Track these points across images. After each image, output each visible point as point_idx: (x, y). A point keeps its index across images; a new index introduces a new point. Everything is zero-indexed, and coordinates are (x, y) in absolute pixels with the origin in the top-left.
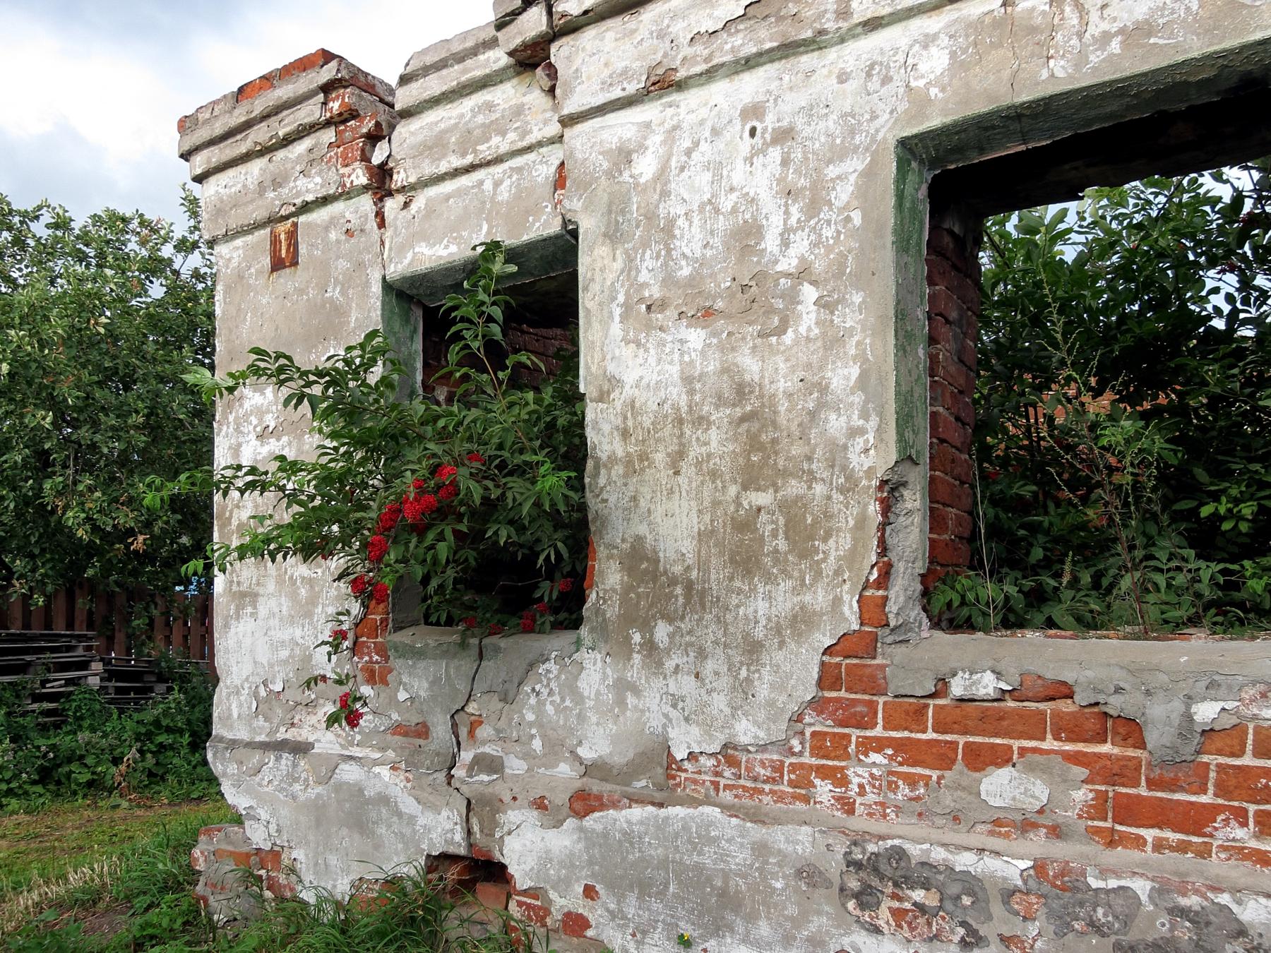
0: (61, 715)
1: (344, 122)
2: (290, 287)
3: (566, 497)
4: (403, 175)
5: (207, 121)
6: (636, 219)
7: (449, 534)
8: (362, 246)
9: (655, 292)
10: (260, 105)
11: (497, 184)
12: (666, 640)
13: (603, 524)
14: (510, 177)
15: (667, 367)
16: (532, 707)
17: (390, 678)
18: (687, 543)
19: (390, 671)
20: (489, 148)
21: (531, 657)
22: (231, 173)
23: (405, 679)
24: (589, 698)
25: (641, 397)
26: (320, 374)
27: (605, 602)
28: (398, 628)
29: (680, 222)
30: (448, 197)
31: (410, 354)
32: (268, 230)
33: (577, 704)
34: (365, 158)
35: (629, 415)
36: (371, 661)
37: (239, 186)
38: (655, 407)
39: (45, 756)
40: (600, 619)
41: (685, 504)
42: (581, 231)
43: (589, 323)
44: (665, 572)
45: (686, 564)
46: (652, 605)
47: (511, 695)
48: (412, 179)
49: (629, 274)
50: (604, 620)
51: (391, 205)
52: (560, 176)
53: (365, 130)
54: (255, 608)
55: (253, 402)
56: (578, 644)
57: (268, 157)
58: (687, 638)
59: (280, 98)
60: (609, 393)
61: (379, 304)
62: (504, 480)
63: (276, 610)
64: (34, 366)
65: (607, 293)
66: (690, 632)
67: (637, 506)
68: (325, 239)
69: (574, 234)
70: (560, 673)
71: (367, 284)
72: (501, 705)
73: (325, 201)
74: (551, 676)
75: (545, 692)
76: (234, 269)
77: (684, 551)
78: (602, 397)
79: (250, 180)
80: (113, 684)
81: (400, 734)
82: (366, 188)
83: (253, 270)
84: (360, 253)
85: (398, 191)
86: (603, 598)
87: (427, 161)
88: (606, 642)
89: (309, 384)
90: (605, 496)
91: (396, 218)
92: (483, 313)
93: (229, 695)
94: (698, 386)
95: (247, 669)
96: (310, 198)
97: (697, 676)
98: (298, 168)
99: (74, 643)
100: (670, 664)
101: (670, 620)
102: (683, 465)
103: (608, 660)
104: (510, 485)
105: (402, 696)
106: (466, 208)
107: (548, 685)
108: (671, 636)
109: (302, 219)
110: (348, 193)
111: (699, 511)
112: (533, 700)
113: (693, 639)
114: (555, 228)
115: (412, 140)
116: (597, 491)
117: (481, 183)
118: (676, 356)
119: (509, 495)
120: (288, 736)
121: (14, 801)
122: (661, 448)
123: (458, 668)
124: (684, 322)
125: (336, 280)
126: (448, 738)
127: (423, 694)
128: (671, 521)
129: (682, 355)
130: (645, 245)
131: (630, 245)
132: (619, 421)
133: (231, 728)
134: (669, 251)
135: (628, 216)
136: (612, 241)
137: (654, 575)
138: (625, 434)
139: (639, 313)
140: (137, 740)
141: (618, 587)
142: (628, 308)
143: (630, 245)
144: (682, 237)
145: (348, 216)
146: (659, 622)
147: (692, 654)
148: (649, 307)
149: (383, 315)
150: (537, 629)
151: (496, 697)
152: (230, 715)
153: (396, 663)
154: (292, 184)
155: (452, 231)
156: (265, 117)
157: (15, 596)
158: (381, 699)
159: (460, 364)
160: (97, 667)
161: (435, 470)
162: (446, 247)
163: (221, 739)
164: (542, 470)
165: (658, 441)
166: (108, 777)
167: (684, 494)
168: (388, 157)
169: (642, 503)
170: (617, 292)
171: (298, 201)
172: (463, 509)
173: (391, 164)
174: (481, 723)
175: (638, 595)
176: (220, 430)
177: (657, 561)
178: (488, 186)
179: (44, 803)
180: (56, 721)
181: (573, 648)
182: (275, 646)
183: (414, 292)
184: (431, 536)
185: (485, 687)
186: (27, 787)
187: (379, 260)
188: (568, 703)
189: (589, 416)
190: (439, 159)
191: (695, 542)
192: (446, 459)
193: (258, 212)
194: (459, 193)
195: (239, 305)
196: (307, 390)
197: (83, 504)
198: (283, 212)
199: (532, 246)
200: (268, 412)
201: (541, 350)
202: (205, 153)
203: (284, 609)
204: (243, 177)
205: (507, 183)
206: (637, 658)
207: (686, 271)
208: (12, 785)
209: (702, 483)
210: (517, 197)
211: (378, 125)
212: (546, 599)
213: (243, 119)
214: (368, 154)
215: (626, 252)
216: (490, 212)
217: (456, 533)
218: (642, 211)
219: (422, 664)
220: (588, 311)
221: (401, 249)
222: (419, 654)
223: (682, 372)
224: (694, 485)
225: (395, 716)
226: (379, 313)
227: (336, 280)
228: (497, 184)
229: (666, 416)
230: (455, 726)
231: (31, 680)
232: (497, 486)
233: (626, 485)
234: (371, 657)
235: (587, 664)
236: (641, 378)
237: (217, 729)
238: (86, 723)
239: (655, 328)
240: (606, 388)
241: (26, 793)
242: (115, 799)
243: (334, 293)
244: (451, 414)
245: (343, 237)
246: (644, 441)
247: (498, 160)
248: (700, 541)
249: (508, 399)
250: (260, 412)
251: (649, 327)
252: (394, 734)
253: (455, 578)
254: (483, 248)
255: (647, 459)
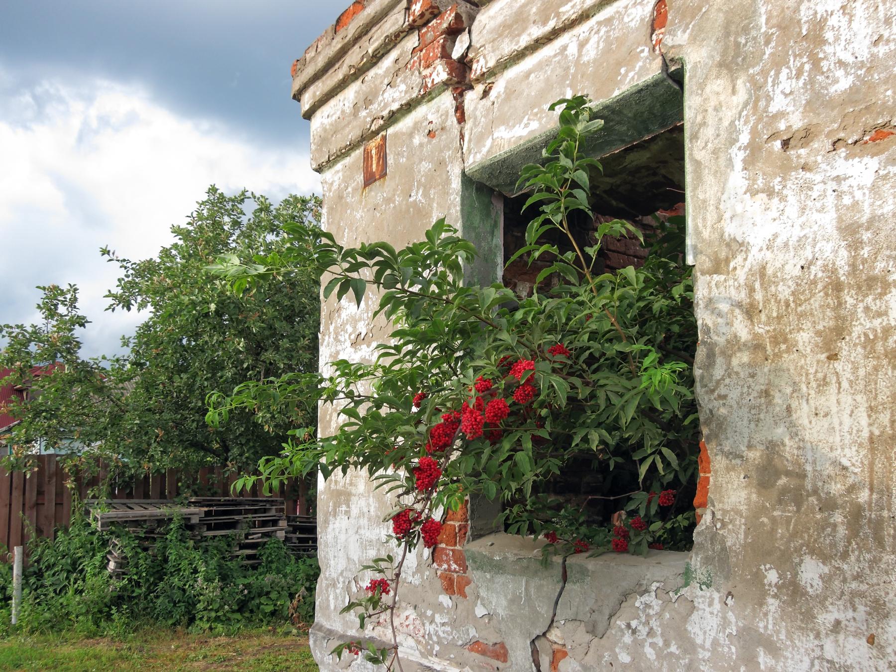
0: (258, 559)
1: (425, 24)
2: (379, 198)
3: (677, 393)
4: (482, 61)
5: (313, 58)
6: (766, 33)
7: (528, 445)
8: (442, 143)
9: (796, 121)
10: (351, 29)
11: (582, 45)
12: (818, 584)
13: (720, 425)
14: (598, 32)
15: (816, 216)
16: (626, 647)
17: (467, 590)
18: (851, 452)
19: (468, 583)
20: (573, 7)
21: (625, 585)
22: (333, 102)
23: (483, 593)
24: (703, 647)
25: (774, 261)
26: (370, 252)
27: (724, 525)
28: (477, 536)
29: (833, 21)
30: (528, 75)
31: (490, 249)
32: (362, 149)
33: (685, 651)
34: (446, 55)
35: (757, 285)
36: (449, 570)
37: (338, 113)
38: (797, 272)
39: (242, 591)
40: (718, 547)
41: (847, 400)
42: (688, 68)
43: (699, 178)
44: (815, 492)
45: (850, 481)
46: (794, 535)
47: (600, 628)
48: (491, 64)
49: (755, 106)
50: (724, 549)
51: (471, 98)
52: (659, 13)
53: (445, 25)
54: (348, 506)
55: (348, 312)
56: (687, 575)
57: (361, 79)
58: (854, 585)
59: (369, 14)
60: (727, 261)
61: (458, 199)
62: (595, 377)
63: (365, 510)
64: (232, 306)
65: (724, 135)
66: (858, 577)
67: (770, 403)
68: (410, 146)
69: (678, 78)
70: (663, 610)
71: (448, 181)
72: (589, 637)
73: (409, 107)
74: (651, 612)
75: (644, 630)
76: (335, 190)
77: (845, 462)
78: (718, 266)
79: (347, 105)
80: (298, 535)
81: (478, 652)
82: (446, 84)
83: (350, 189)
84: (441, 151)
85: (478, 80)
86: (722, 521)
87: (507, 40)
88: (727, 578)
89: (355, 267)
90: (722, 390)
91: (476, 109)
92: (566, 180)
93: (327, 586)
94: (866, 236)
95: (342, 564)
96: (395, 107)
97: (871, 640)
98: (386, 82)
99: (268, 506)
100: (825, 618)
101: (825, 558)
102: (844, 347)
103: (730, 601)
104: (602, 382)
105: (480, 611)
106: (547, 79)
107: (647, 623)
108: (827, 580)
109: (391, 131)
110: (430, 93)
111: (871, 408)
112: (628, 639)
113: (864, 587)
114: (653, 71)
115: (492, 24)
116: (711, 385)
117: (564, 48)
118: (831, 199)
119: (601, 394)
120: (375, 634)
121: (220, 625)
122: (807, 325)
123: (539, 588)
124: (842, 152)
125: (419, 182)
126: (528, 666)
127: (501, 612)
128: (825, 423)
129: (839, 195)
130: (779, 62)
131: (757, 69)
132: (743, 296)
133: (328, 618)
134: (816, 63)
135: (754, 33)
136: (730, 70)
137: (797, 496)
138: (750, 311)
139: (770, 153)
140: (307, 580)
141: (743, 508)
142: (754, 151)
143: (757, 69)
144: (837, 39)
145: (431, 117)
146: (807, 559)
147: (861, 609)
148: (786, 144)
149: (462, 210)
150: (631, 549)
151: (582, 628)
152: (328, 606)
153: (474, 575)
154: (380, 98)
155: (532, 108)
156: (356, 39)
157: (228, 473)
158: (459, 611)
159: (539, 243)
160: (283, 524)
161: (507, 366)
162: (526, 125)
163: (320, 628)
164: (647, 362)
165: (801, 316)
166: (286, 608)
167: (845, 385)
168: (468, 48)
169: (778, 400)
170: (739, 132)
171: (385, 113)
172: (544, 412)
173: (471, 55)
174: (565, 654)
175: (774, 520)
176: (324, 340)
177: (803, 476)
178: (572, 50)
179: (239, 629)
180: (254, 564)
181: (680, 581)
182: (365, 545)
183: (494, 182)
184: (506, 445)
185: (570, 614)
186: (229, 615)
187: (459, 155)
188: (673, 648)
189: (701, 293)
190: (519, 35)
191: (863, 452)
192: (521, 351)
193: (352, 134)
194: (540, 66)
195: (339, 223)
196: (354, 275)
197: (269, 407)
198: (373, 128)
199: (624, 102)
200: (360, 319)
201: (623, 249)
202: (312, 89)
203: (372, 509)
204: (341, 104)
205: (594, 39)
206: (773, 604)
207: (844, 83)
208: (219, 614)
209: (876, 369)
210: (607, 51)
211: (458, 17)
212: (642, 513)
213: (339, 46)
214: (448, 50)
215: (752, 80)
216: (574, 76)
217: (536, 440)
218: (774, 21)
219: (500, 579)
220: (698, 164)
221: (480, 139)
222: (498, 568)
223: (840, 219)
224: (862, 372)
225: (473, 632)
226: (458, 208)
227: (419, 182)
228: (582, 45)
229: (814, 282)
230: (535, 653)
231: (239, 533)
232: (587, 384)
233: (752, 376)
234: (449, 566)
235: (697, 602)
236: (776, 236)
237: (319, 618)
238: (274, 566)
239: (795, 169)
240: (723, 255)
241: (229, 619)
242: (287, 626)
243: (417, 196)
244: (531, 304)
245: (426, 140)
246: (779, 318)
247: (584, 16)
248: (872, 450)
249: (598, 280)
250: (354, 321)
251: (785, 168)
252: (471, 650)
253: (534, 482)
254: (564, 105)
255: (785, 341)
